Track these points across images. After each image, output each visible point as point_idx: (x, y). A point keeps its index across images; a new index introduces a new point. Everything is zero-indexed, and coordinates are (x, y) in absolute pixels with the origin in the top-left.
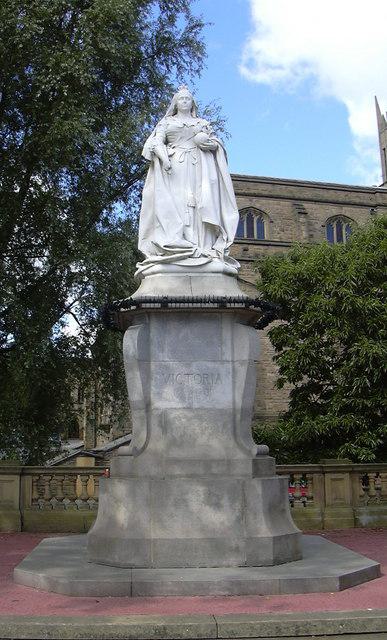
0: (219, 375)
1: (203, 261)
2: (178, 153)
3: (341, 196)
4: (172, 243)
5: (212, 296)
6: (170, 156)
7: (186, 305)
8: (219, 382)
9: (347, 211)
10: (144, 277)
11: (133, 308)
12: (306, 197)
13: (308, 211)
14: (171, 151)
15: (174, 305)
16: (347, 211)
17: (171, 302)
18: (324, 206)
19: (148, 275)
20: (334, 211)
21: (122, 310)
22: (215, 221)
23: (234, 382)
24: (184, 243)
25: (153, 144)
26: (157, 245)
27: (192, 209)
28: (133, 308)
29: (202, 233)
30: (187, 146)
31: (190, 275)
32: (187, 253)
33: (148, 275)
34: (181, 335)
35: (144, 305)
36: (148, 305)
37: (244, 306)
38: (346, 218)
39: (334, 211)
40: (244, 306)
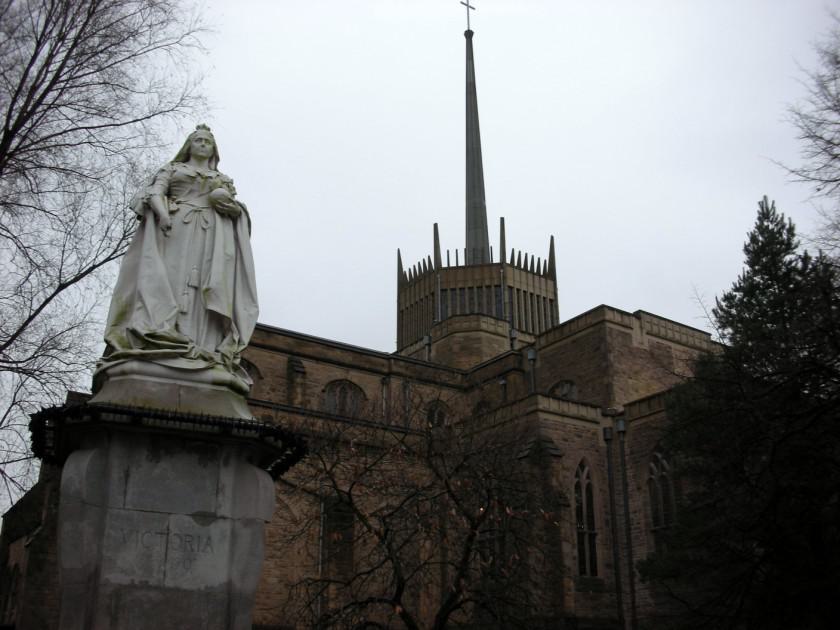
0: (209, 538)
1: (202, 364)
2: (184, 209)
3: (348, 358)
4: (160, 332)
5: (206, 413)
6: (172, 213)
7: (171, 423)
8: (209, 549)
9: (354, 376)
10: (108, 376)
11: (86, 418)
12: (307, 353)
13: (308, 370)
14: (174, 207)
15: (151, 421)
16: (354, 376)
17: (148, 415)
18: (329, 367)
19: (115, 375)
20: (338, 373)
21: (69, 419)
22: (226, 312)
23: (232, 553)
24: (175, 335)
25: (37, 463)
26: (134, 333)
27: (192, 292)
28: (86, 418)
29: (204, 327)
30: (198, 202)
31: (179, 382)
32: (178, 348)
33: (115, 375)
34: (157, 471)
35: (104, 416)
36: (111, 417)
37: (257, 436)
38: (352, 385)
39: (338, 373)
40: (257, 436)
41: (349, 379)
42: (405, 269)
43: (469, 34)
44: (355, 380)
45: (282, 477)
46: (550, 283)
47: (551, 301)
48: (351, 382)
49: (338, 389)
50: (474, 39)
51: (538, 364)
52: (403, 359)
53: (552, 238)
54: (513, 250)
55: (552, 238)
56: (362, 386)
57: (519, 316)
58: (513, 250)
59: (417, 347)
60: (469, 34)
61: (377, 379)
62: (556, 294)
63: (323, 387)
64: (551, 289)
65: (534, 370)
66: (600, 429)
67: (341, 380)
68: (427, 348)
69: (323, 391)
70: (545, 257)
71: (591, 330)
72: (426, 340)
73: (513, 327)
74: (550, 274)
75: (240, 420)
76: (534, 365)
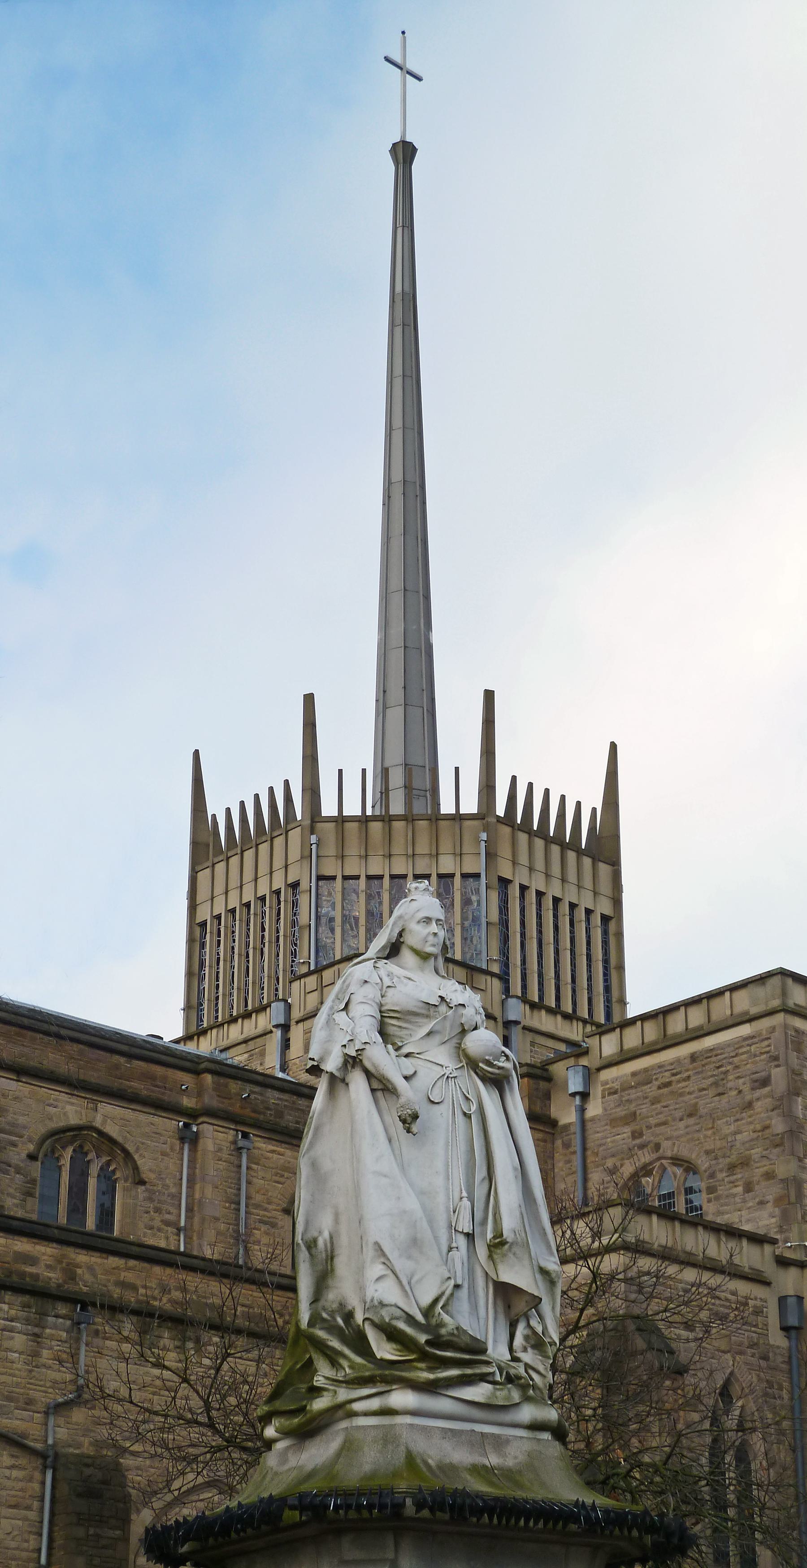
16: (111, 1117)
20: (70, 1110)
39: (70, 1110)
41: (98, 1123)
42: (215, 807)
43: (404, 153)
44: (112, 1130)
45: (282, 1524)
46: (604, 869)
47: (605, 919)
48: (100, 1133)
49: (69, 1151)
50: (418, 166)
51: (594, 1109)
52: (194, 1066)
53: (613, 747)
54: (514, 779)
55: (613, 747)
56: (131, 1148)
57: (524, 962)
58: (514, 779)
59: (249, 1028)
60: (404, 153)
61: (171, 1125)
62: (617, 903)
63: (31, 1147)
64: (605, 887)
65: (583, 1122)
66: (767, 1297)
67: (79, 1128)
68: (278, 1033)
69: (32, 1157)
70: (593, 799)
71: (745, 1030)
72: (276, 1013)
73: (507, 991)
74: (602, 846)
75: (464, 1493)
76: (582, 1110)
